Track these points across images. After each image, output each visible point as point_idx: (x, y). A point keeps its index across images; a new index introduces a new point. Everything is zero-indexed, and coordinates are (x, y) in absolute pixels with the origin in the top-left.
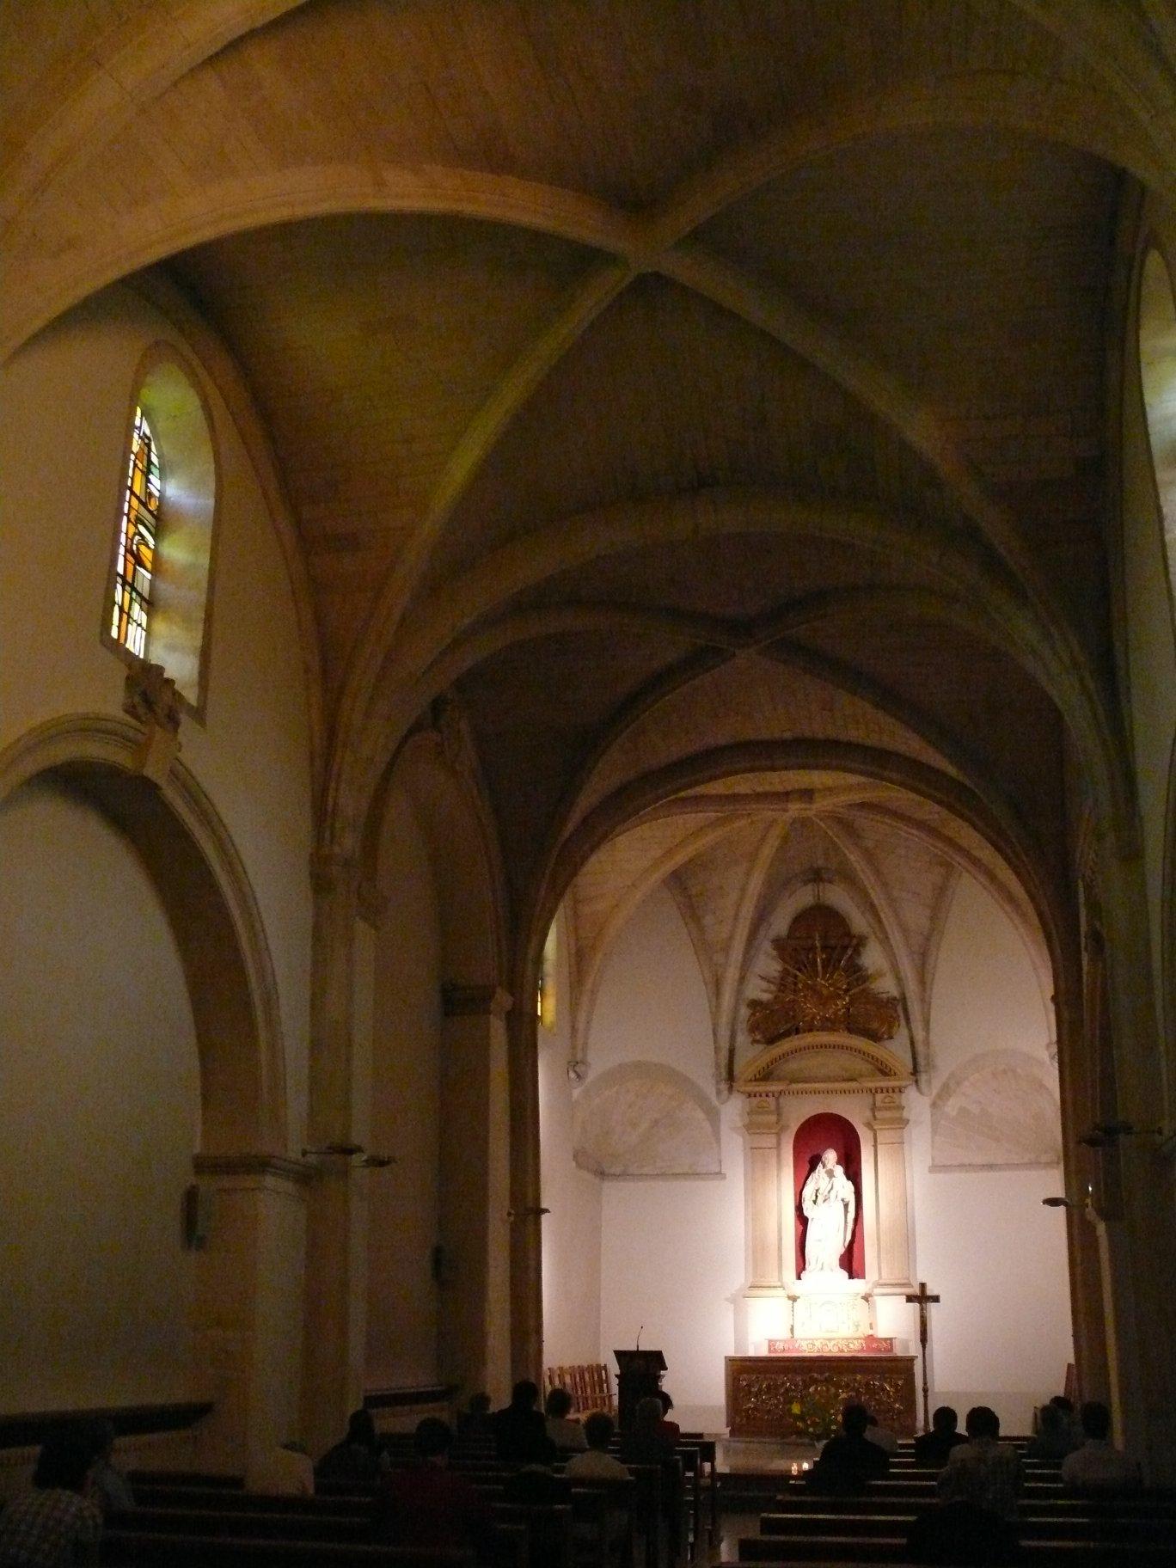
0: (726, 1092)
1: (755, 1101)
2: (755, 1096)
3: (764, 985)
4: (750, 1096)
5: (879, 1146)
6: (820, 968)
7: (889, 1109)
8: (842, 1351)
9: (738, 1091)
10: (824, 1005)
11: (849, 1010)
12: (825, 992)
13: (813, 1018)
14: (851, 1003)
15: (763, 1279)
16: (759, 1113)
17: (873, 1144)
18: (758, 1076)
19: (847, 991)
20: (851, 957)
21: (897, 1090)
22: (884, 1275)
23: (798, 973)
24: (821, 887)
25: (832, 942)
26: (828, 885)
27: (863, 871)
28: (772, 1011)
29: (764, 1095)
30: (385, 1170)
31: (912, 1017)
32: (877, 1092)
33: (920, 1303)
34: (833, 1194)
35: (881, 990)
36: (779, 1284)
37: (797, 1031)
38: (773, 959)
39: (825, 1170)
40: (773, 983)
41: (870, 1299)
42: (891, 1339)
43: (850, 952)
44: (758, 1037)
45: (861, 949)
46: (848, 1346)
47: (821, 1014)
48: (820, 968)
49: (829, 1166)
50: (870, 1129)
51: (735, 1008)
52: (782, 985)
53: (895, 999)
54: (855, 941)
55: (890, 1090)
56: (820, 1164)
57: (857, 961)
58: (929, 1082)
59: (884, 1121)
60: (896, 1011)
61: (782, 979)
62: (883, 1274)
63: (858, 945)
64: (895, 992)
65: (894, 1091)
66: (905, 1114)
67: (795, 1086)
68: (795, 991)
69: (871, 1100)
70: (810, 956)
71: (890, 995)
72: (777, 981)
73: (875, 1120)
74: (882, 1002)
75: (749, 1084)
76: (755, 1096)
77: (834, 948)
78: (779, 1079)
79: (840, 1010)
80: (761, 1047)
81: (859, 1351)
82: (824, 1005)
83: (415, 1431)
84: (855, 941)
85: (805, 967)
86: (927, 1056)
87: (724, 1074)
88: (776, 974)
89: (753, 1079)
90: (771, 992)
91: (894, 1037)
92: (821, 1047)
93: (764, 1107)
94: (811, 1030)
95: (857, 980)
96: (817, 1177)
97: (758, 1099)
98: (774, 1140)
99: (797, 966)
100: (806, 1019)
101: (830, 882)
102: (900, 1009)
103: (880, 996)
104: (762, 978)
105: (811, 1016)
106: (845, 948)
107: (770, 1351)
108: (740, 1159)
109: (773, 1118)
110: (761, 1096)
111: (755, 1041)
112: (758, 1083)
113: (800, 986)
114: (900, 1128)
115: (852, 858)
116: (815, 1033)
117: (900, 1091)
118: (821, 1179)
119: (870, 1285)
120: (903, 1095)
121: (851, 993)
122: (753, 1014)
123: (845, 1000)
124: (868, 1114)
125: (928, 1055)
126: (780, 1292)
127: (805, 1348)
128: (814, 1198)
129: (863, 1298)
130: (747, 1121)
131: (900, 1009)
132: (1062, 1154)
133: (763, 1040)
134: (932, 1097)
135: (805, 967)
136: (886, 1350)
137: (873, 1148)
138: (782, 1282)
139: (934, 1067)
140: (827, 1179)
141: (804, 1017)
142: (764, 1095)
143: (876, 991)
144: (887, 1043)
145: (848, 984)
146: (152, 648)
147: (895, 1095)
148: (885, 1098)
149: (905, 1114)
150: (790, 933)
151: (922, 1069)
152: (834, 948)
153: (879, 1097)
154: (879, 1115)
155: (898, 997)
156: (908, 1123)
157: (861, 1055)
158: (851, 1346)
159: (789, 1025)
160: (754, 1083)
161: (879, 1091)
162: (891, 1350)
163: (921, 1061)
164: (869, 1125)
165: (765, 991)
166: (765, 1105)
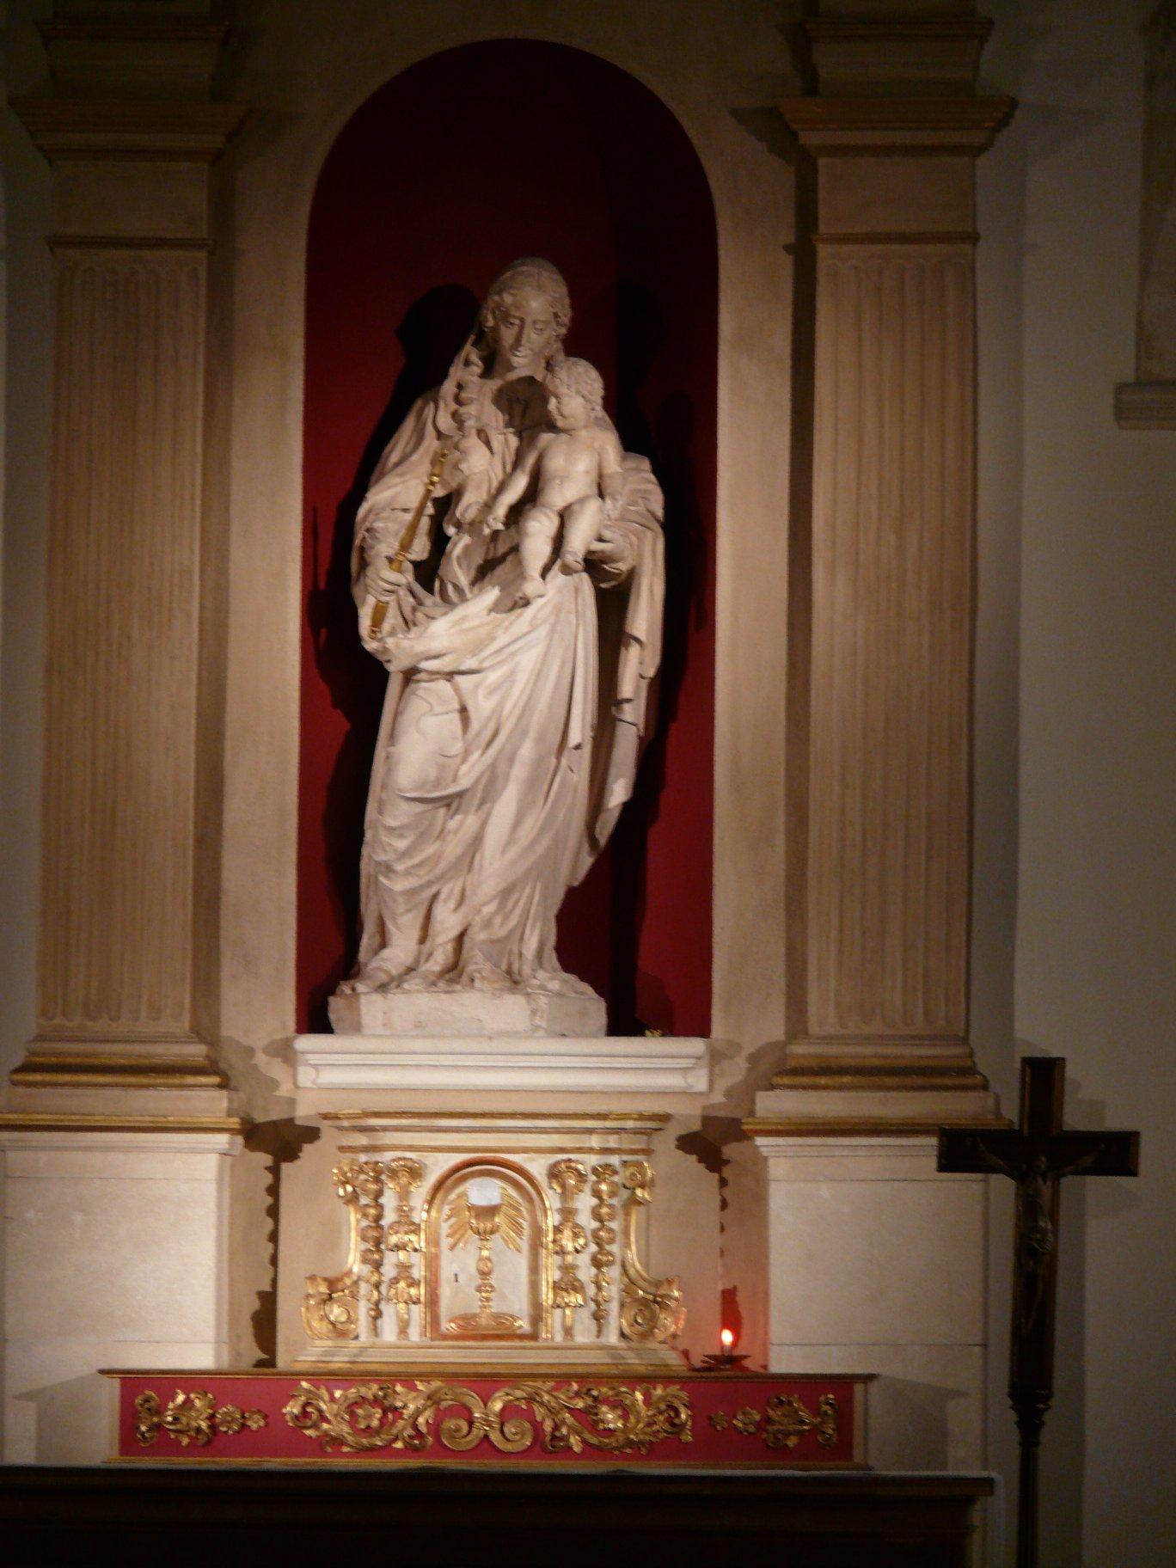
5: (823, 251)
8: (551, 1445)
15: (102, 1025)
17: (789, 237)
22: (822, 1013)
30: (725, 1224)
33: (1023, 1176)
34: (538, 532)
36: (196, 1052)
39: (494, 384)
41: (730, 1150)
42: (842, 1384)
46: (588, 1419)
49: (523, 364)
56: (470, 351)
62: (813, 1008)
73: (811, 87)
81: (653, 1450)
96: (445, 422)
107: (128, 1438)
114: (958, 150)
118: (473, 443)
119: (736, 1071)
126: (210, 1102)
127: (337, 1427)
128: (421, 548)
129: (688, 1143)
132: (781, 791)
136: (810, 1446)
137: (786, 266)
138: (213, 1041)
140: (506, 441)
146: (205, 1120)
154: (830, 61)
156: (1004, 122)
158: (611, 1418)
162: (842, 1448)
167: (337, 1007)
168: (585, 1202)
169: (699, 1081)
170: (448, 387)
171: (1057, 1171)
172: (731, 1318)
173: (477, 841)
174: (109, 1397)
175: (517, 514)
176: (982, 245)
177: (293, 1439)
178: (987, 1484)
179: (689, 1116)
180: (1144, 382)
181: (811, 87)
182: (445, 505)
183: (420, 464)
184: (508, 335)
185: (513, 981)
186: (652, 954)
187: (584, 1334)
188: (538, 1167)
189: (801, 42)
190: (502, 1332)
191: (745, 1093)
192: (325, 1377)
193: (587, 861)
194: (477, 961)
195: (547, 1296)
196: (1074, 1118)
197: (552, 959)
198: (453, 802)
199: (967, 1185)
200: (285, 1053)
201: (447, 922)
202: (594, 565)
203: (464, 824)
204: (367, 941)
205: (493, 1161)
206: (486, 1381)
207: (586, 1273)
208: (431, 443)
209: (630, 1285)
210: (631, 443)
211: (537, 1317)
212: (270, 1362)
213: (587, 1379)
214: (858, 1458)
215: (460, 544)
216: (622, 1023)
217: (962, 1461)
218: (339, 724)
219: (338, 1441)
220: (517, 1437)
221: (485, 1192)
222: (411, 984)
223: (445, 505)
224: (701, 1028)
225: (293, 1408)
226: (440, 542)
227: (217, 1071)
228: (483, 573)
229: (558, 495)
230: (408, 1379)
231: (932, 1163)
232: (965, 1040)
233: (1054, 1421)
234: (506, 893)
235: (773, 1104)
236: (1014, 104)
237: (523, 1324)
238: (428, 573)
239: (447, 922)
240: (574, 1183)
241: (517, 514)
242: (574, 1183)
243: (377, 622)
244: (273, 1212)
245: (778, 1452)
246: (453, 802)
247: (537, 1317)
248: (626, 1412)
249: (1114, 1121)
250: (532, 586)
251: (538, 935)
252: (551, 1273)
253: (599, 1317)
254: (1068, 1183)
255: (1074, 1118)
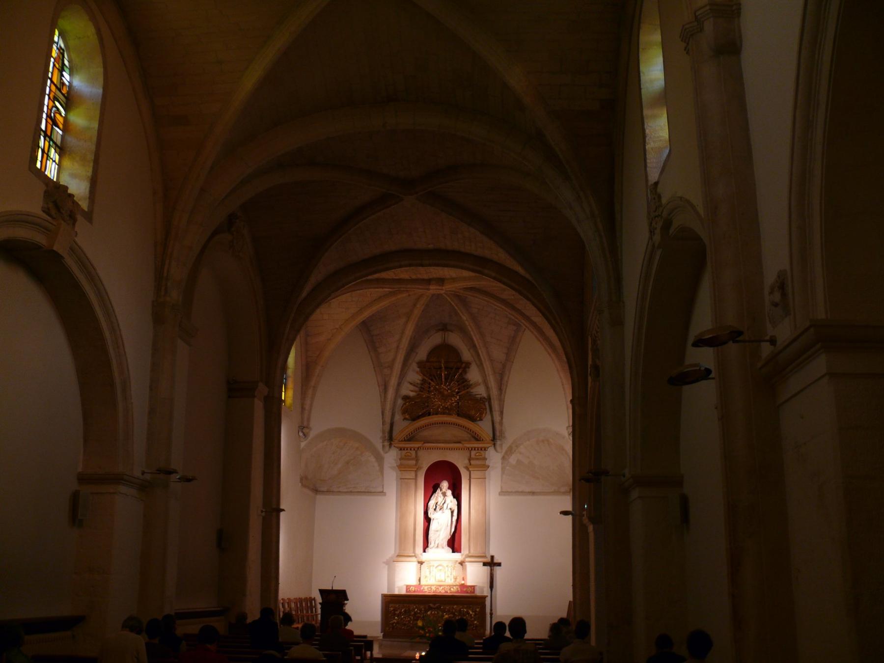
5: (472, 480)
8: (447, 592)
17: (468, 478)
22: (472, 551)
33: (491, 567)
34: (445, 506)
36: (413, 555)
41: (463, 564)
46: (450, 589)
49: (444, 490)
73: (470, 464)
81: (456, 592)
96: (437, 495)
107: (407, 591)
119: (464, 556)
126: (414, 559)
127: (426, 590)
128: (434, 507)
136: (471, 592)
137: (468, 481)
154: (472, 462)
156: (488, 468)
162: (474, 592)
167: (426, 550)
168: (450, 569)
169: (460, 557)
170: (437, 492)
171: (494, 566)
172: (463, 580)
173: (439, 535)
174: (405, 587)
175: (443, 504)
176: (487, 479)
177: (422, 591)
178: (487, 596)
179: (459, 561)
180: (501, 492)
181: (470, 464)
182: (437, 503)
183: (434, 499)
184: (442, 487)
185: (443, 548)
186: (456, 546)
187: (449, 581)
188: (445, 565)
189: (469, 460)
190: (442, 581)
191: (465, 558)
192: (426, 586)
193: (450, 537)
194: (440, 546)
195: (446, 578)
196: (495, 561)
197: (447, 546)
198: (437, 531)
199: (486, 568)
200: (421, 554)
201: (437, 543)
202: (450, 509)
203: (438, 533)
204: (429, 544)
205: (426, 533)
206: (441, 586)
207: (450, 575)
208: (435, 497)
209: (454, 577)
210: (454, 497)
211: (445, 580)
212: (420, 584)
213: (450, 586)
214: (475, 593)
215: (438, 507)
216: (453, 552)
217: (485, 594)
218: (427, 524)
219: (426, 592)
220: (443, 591)
221: (440, 568)
222: (434, 548)
223: (437, 503)
224: (460, 552)
225: (422, 588)
226: (436, 507)
227: (415, 556)
228: (440, 509)
229: (447, 502)
230: (433, 586)
231: (386, 592)
232: (485, 553)
233: (494, 590)
234: (442, 540)
235: (468, 559)
236: (489, 466)
237: (444, 580)
238: (435, 510)
239: (437, 543)
240: (474, 411)
241: (443, 504)
242: (474, 411)
243: (430, 513)
244: (420, 570)
245: (468, 593)
246: (437, 531)
247: (445, 580)
248: (454, 589)
249: (499, 561)
250: (444, 511)
251: (445, 543)
252: (446, 575)
253: (451, 580)
254: (495, 567)
255: (495, 561)
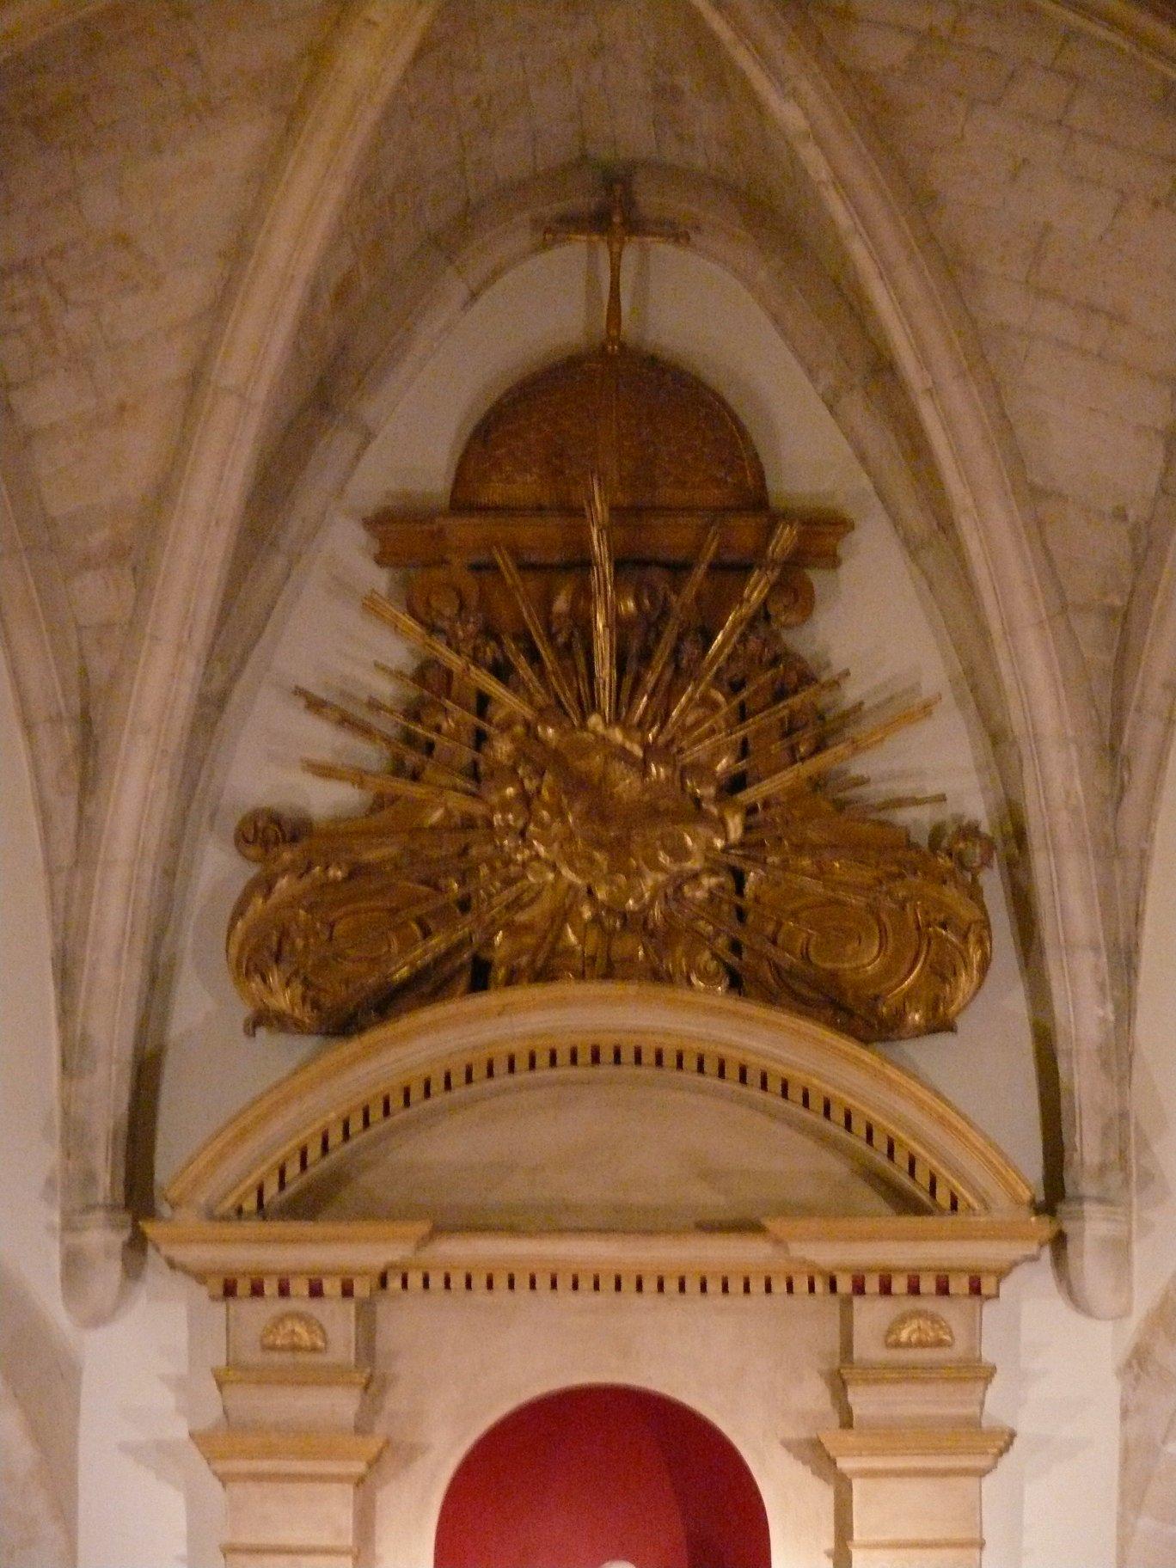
0: (114, 1270)
1: (256, 1315)
2: (257, 1291)
3: (324, 738)
4: (229, 1290)
6: (605, 671)
7: (907, 1374)
9: (172, 1264)
10: (619, 850)
11: (739, 877)
12: (626, 784)
13: (563, 914)
14: (751, 846)
16: (264, 1378)
17: (829, 1543)
18: (271, 1190)
19: (737, 783)
20: (763, 615)
21: (959, 1285)
23: (494, 687)
24: (630, 256)
25: (671, 537)
26: (662, 249)
27: (840, 181)
28: (356, 871)
29: (300, 1287)
31: (1048, 930)
32: (859, 1288)
35: (904, 788)
37: (480, 978)
38: (370, 606)
40: (366, 731)
43: (755, 591)
44: (283, 1000)
45: (816, 577)
47: (601, 894)
48: (605, 671)
50: (818, 1473)
51: (244, 855)
52: (410, 739)
53: (969, 832)
54: (785, 538)
55: (928, 1285)
57: (788, 637)
58: (1120, 1249)
59: (891, 1436)
60: (974, 893)
61: (414, 713)
63: (797, 561)
64: (977, 808)
65: (943, 1289)
66: (997, 1404)
67: (459, 1251)
68: (474, 773)
69: (833, 1328)
70: (561, 604)
71: (945, 814)
72: (388, 725)
74: (910, 845)
75: (230, 1230)
76: (257, 1291)
77: (678, 569)
78: (373, 1212)
79: (695, 877)
80: (305, 1046)
82: (619, 850)
83: (304, 839)
84: (785, 538)
85: (534, 657)
86: (1119, 1123)
87: (106, 1179)
88: (386, 689)
89: (250, 1204)
90: (358, 777)
91: (960, 1022)
92: (596, 1058)
93: (295, 1348)
94: (544, 974)
95: (789, 730)
97: (270, 1307)
98: (338, 1507)
99: (490, 652)
100: (522, 917)
101: (678, 234)
102: (992, 883)
103: (904, 816)
104: (315, 705)
105: (546, 904)
106: (735, 570)
108: (274, 966)
109: (343, 1404)
110: (284, 1291)
111: (262, 1019)
112: (277, 1228)
113: (503, 748)
115: (789, 115)
116: (568, 988)
117: (975, 1289)
120: (989, 1309)
121: (749, 795)
122: (264, 885)
123: (721, 826)
124: (814, 1395)
125: (1124, 1115)
130: (211, 1410)
131: (992, 883)
133: (304, 1014)
134: (1134, 1323)
135: (534, 657)
139: (1147, 1178)
141: (516, 905)
142: (300, 1287)
143: (876, 792)
144: (926, 1054)
145: (744, 750)
147: (942, 1307)
148: (903, 1320)
149: (997, 1404)
150: (461, 477)
151: (1089, 1188)
152: (678, 569)
153: (871, 1315)
155: (985, 828)
157: (814, 1118)
159: (438, 943)
160: (253, 1227)
161: (872, 1285)
163: (1087, 1146)
164: (818, 1457)
165: (324, 771)
166: (304, 1335)
